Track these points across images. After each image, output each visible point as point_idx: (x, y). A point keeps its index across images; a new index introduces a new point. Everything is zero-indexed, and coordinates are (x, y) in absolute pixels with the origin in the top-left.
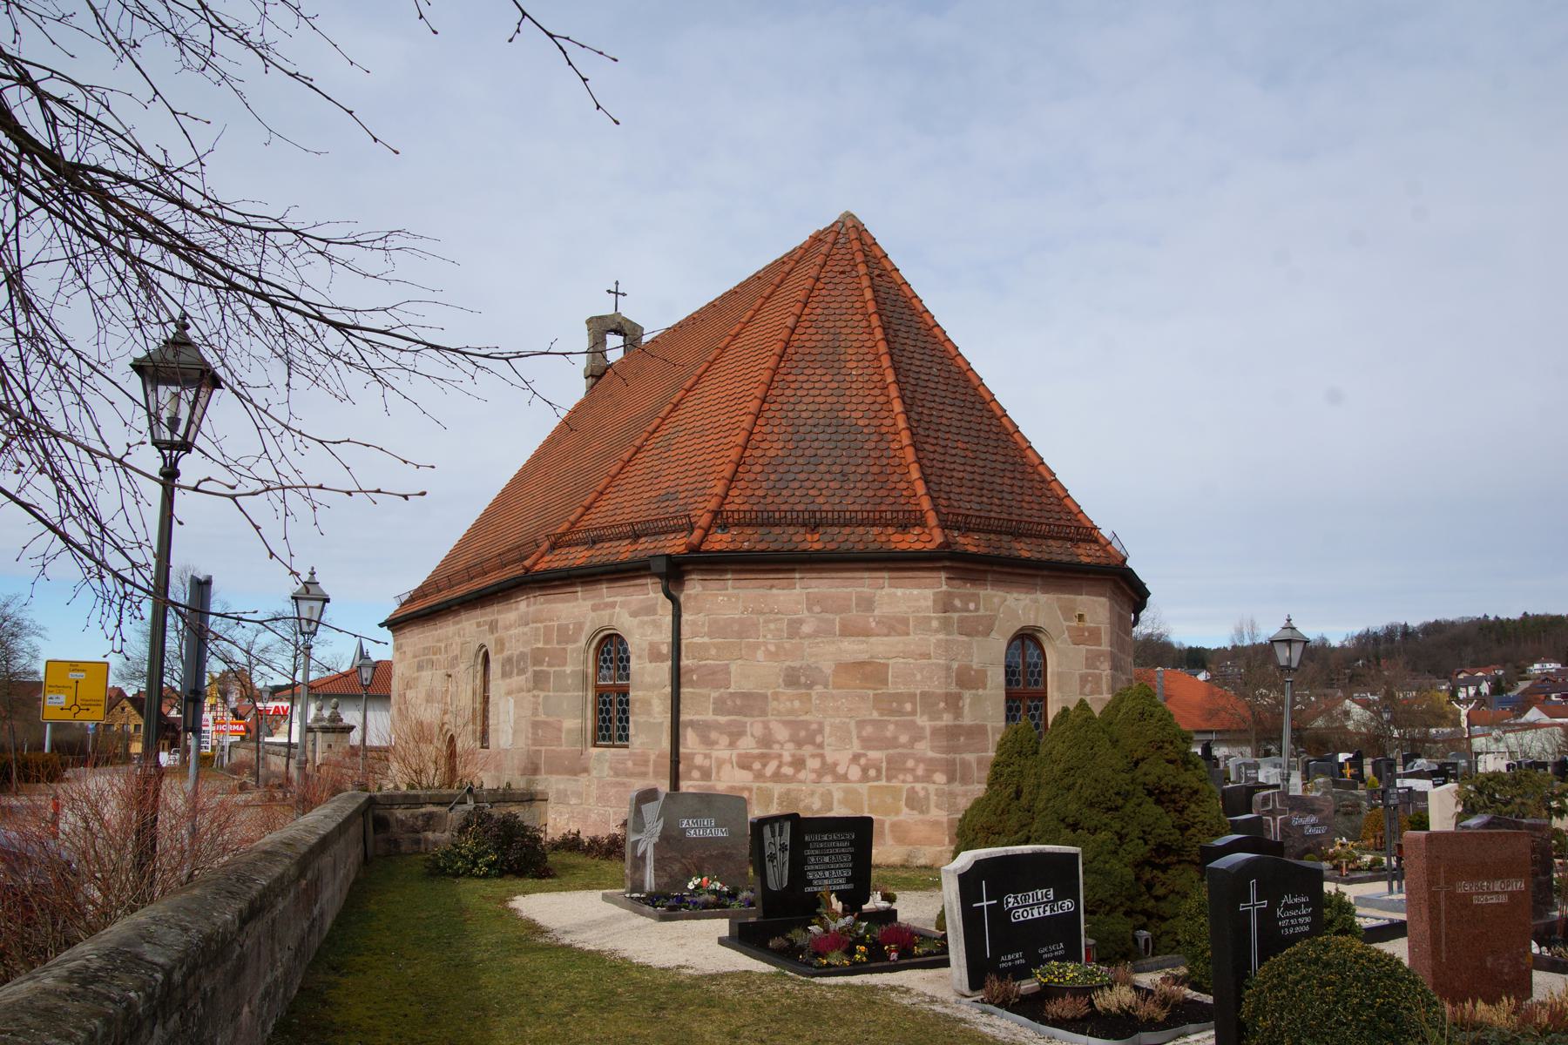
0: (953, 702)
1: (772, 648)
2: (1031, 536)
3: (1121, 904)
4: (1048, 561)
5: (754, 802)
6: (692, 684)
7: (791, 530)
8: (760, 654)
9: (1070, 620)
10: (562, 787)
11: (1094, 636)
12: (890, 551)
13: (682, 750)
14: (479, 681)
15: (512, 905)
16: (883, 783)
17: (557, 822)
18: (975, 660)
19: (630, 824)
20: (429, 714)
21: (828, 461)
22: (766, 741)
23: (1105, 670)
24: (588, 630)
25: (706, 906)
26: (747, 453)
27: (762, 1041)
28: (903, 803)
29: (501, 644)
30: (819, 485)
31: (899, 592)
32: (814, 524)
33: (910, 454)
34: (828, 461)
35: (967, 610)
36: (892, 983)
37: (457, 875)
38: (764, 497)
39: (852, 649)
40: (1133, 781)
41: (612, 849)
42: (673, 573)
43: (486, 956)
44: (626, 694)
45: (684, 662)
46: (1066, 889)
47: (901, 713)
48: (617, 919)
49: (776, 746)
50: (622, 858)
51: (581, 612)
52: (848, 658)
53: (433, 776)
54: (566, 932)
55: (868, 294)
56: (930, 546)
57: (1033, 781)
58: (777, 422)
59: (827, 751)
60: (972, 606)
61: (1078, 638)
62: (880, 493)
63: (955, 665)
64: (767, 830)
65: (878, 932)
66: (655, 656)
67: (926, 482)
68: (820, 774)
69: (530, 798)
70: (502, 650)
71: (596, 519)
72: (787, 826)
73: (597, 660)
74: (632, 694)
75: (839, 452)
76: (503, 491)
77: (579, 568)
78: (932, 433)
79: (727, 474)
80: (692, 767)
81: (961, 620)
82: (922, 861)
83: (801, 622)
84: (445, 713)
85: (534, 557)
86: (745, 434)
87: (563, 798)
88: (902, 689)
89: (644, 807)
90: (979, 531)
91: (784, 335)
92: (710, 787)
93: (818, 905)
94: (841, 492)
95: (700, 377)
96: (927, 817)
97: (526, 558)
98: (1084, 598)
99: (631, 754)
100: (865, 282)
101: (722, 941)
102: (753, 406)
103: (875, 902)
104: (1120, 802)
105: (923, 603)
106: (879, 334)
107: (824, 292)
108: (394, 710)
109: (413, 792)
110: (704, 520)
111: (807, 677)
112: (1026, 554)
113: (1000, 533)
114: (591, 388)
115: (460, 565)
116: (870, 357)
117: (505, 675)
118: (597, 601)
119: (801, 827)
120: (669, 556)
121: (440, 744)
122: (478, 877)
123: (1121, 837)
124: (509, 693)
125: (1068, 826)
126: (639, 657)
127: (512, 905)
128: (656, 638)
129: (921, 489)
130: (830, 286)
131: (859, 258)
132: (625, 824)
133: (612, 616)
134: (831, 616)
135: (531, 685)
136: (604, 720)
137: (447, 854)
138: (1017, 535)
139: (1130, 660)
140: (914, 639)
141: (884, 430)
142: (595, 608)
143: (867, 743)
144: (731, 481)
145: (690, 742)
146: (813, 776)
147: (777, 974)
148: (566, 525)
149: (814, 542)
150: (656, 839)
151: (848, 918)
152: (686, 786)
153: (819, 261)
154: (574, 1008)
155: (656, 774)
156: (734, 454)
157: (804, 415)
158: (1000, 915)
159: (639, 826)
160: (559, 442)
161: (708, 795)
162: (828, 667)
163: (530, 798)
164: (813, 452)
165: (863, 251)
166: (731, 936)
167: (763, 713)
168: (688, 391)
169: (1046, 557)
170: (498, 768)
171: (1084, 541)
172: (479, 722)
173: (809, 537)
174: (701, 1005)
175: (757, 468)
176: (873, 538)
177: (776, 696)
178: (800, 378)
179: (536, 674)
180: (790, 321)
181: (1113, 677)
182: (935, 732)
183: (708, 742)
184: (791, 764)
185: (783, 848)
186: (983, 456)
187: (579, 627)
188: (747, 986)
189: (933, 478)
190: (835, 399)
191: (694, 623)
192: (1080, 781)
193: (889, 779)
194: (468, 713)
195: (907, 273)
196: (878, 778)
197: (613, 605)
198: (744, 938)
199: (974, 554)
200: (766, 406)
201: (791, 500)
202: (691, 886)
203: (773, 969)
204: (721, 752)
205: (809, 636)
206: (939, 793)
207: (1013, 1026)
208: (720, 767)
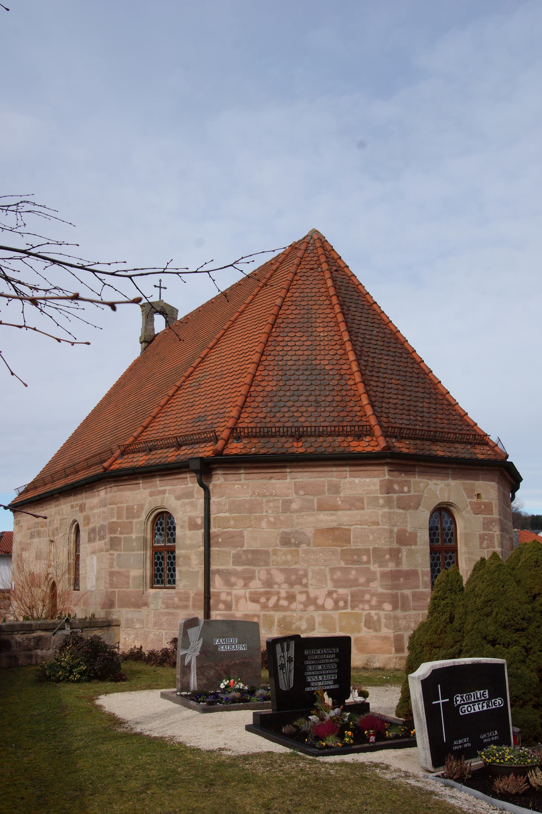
0: (395, 554)
1: (272, 520)
2: (443, 441)
3: (531, 700)
4: (456, 458)
5: (261, 625)
6: (218, 544)
7: (283, 440)
8: (264, 524)
9: (471, 497)
10: (129, 616)
11: (488, 508)
12: (350, 453)
13: (212, 590)
14: (72, 545)
15: (98, 702)
16: (349, 610)
17: (126, 641)
18: (409, 526)
19: (179, 643)
20: (38, 568)
21: (307, 393)
22: (269, 583)
23: (496, 531)
25: (234, 700)
26: (252, 389)
27: (289, 812)
28: (363, 624)
29: (87, 519)
30: (301, 409)
31: (357, 480)
32: (298, 435)
33: (361, 388)
34: (307, 393)
35: (403, 492)
36: (375, 761)
37: (58, 681)
38: (265, 418)
40: (533, 609)
41: (165, 659)
42: (205, 470)
43: (81, 744)
44: (173, 552)
45: (213, 530)
46: (497, 691)
47: (360, 562)
48: (171, 712)
49: (276, 586)
50: (174, 665)
51: (143, 497)
52: (325, 526)
53: (41, 611)
54: (137, 723)
55: (330, 283)
56: (377, 449)
57: (461, 610)
58: (271, 368)
59: (311, 589)
60: (406, 489)
61: (478, 510)
62: (342, 414)
63: (396, 529)
64: (278, 647)
65: (358, 720)
66: (193, 526)
67: (373, 406)
68: (306, 605)
69: (108, 624)
70: (88, 524)
71: (152, 434)
72: (292, 644)
73: (153, 529)
74: (177, 552)
75: (314, 388)
76: (87, 418)
77: (140, 467)
78: (374, 373)
79: (239, 403)
80: (219, 601)
81: (399, 499)
82: (377, 665)
83: (291, 501)
84: (49, 566)
85: (110, 461)
86: (250, 376)
87: (130, 624)
88: (360, 546)
89: (189, 631)
90: (409, 438)
91: (275, 310)
92: (232, 615)
93: (315, 700)
94: (316, 414)
95: (218, 340)
96: (379, 634)
97: (104, 461)
98: (481, 483)
99: (177, 593)
100: (327, 275)
101: (248, 728)
102: (256, 358)
103: (354, 698)
104: (525, 625)
105: (372, 487)
106: (337, 309)
107: (300, 282)
108: (14, 566)
109: (28, 622)
110: (225, 434)
112: (441, 454)
113: (423, 439)
114: (144, 350)
115: (59, 467)
116: (332, 324)
117: (90, 540)
118: (153, 489)
119: (303, 645)
120: (201, 458)
121: (46, 588)
122: (73, 682)
123: (527, 650)
124: (93, 553)
125: (489, 642)
126: (182, 527)
127: (98, 702)
128: (194, 514)
129: (369, 411)
130: (304, 278)
131: (323, 259)
132: (175, 641)
133: (163, 500)
134: (311, 497)
135: (108, 547)
136: (158, 570)
137: (51, 667)
138: (434, 441)
139: (511, 524)
140: (368, 512)
141: (343, 372)
142: (151, 494)
143: (337, 583)
144: (242, 408)
146: (302, 606)
147: (292, 754)
148: (131, 439)
149: (299, 448)
150: (197, 653)
151: (337, 710)
152: (215, 615)
153: (296, 261)
154: (147, 786)
155: (194, 606)
156: (243, 390)
157: (289, 363)
158: (451, 709)
159: (186, 645)
160: (124, 386)
161: (233, 622)
162: (309, 532)
163: (108, 624)
164: (296, 388)
165: (325, 254)
166: (255, 724)
167: (267, 564)
168: (211, 349)
169: (455, 455)
170: (86, 603)
171: (479, 444)
172: (72, 573)
173: (295, 444)
174: (239, 781)
175: (259, 399)
176: (338, 444)
177: (275, 552)
178: (287, 339)
179: (112, 539)
180: (278, 302)
181: (502, 536)
182: (384, 575)
183: (229, 584)
184: (286, 598)
185: (290, 660)
186: (409, 389)
187: (141, 507)
188: (271, 764)
189: (377, 404)
190: (310, 352)
191: (219, 503)
192: (496, 610)
193: (353, 608)
194: (65, 567)
195: (354, 269)
196: (345, 607)
197: (164, 492)
198: (262, 726)
199: (406, 454)
200: (264, 358)
201: (283, 420)
202: (222, 686)
203: (288, 750)
204: (238, 591)
205: (296, 511)
206: (387, 617)
207: (471, 798)
208: (238, 602)
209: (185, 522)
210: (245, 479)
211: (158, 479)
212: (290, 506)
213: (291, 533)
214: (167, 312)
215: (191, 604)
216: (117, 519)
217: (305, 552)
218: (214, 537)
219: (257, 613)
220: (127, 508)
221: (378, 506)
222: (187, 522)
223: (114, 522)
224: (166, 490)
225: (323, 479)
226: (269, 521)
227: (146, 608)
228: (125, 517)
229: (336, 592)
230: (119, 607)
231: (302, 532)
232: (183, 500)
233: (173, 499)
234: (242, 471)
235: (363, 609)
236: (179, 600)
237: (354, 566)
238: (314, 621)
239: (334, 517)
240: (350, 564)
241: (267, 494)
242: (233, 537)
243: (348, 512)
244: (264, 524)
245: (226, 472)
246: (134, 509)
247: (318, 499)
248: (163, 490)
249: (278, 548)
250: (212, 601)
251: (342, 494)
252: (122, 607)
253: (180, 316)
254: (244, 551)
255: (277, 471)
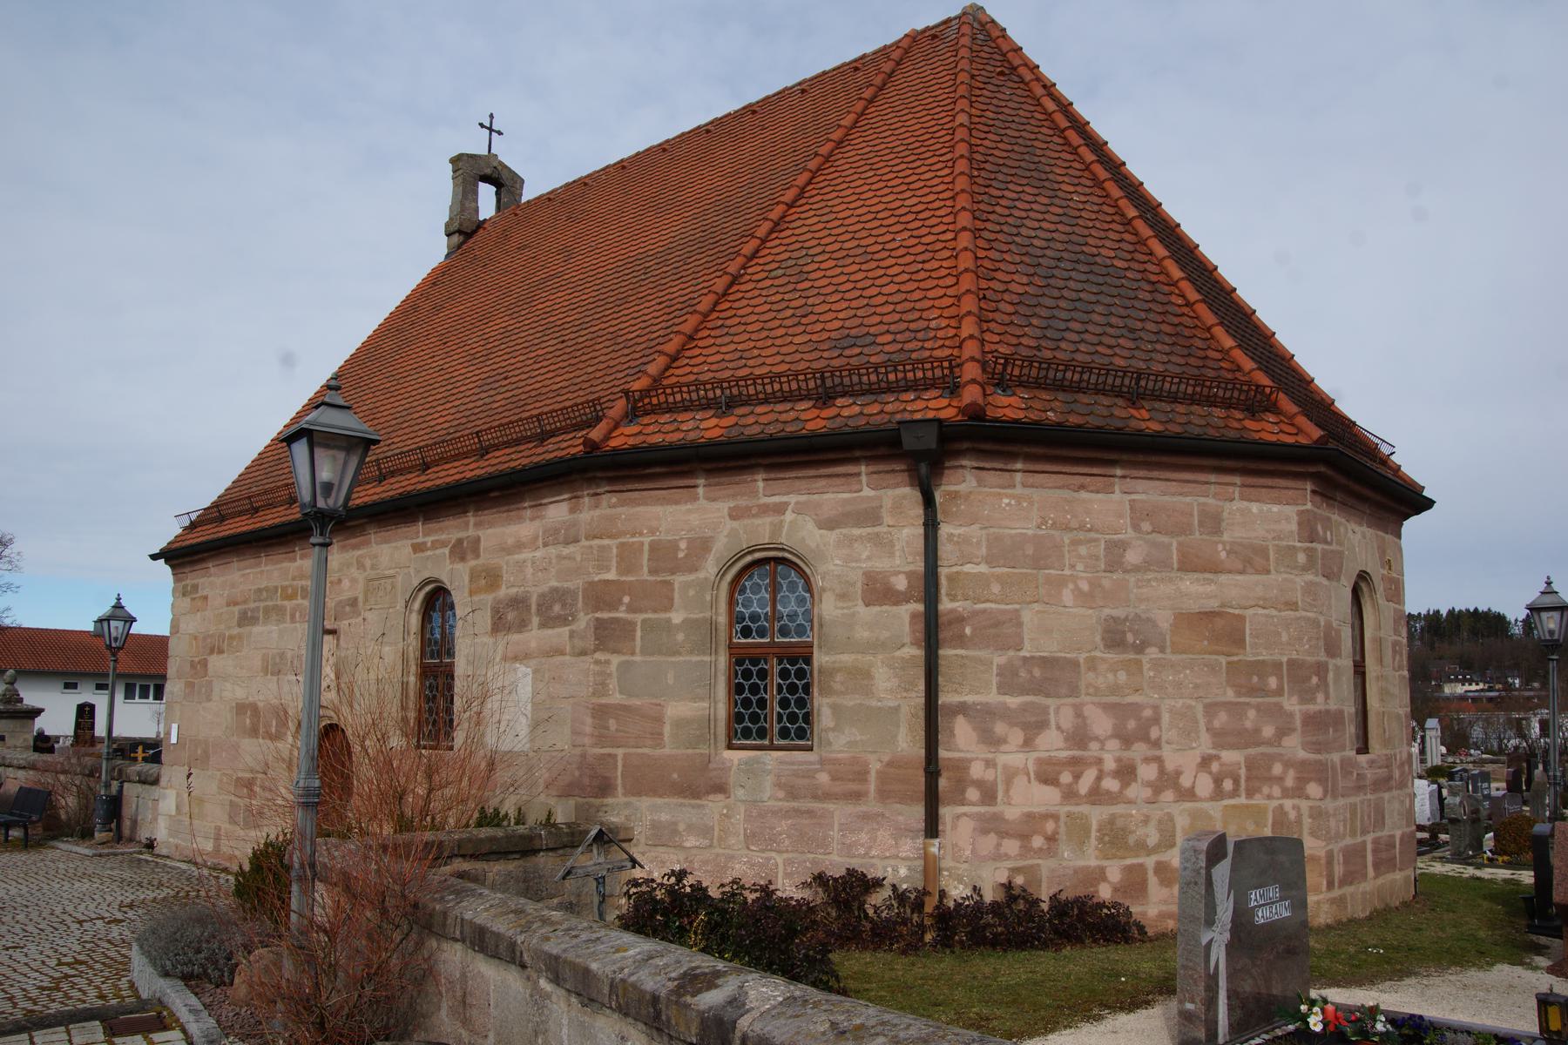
1: (1085, 587)
6: (961, 640)
8: (1067, 596)
10: (664, 817)
13: (943, 753)
16: (1242, 800)
22: (1079, 737)
24: (722, 547)
31: (1255, 507)
39: (1197, 591)
45: (945, 605)
47: (1261, 691)
49: (1094, 746)
51: (708, 521)
52: (1194, 606)
59: (1167, 753)
66: (878, 592)
68: (1157, 788)
74: (820, 659)
83: (1123, 546)
88: (1265, 656)
99: (822, 762)
111: (1136, 633)
118: (742, 502)
128: (881, 564)
133: (777, 529)
135: (591, 642)
142: (735, 515)
143: (1222, 738)
145: (961, 740)
146: (1147, 793)
162: (1164, 619)
167: (1074, 691)
177: (1092, 665)
179: (600, 625)
183: (991, 740)
193: (1250, 794)
196: (1235, 793)
197: (780, 509)
204: (1012, 757)
205: (1136, 569)
209: (853, 584)
210: (1024, 486)
211: (760, 476)
212: (1122, 556)
213: (1126, 619)
214: (503, 180)
215: (872, 787)
216: (621, 572)
217: (1157, 665)
218: (950, 623)
219: (1053, 809)
220: (654, 547)
221: (1295, 568)
222: (859, 585)
223: (607, 581)
224: (787, 504)
225: (1188, 499)
226: (1077, 588)
227: (720, 797)
228: (645, 569)
229: (1218, 758)
230: (625, 795)
231: (1149, 619)
232: (844, 531)
233: (811, 525)
234: (1019, 466)
235: (1269, 797)
236: (834, 779)
237: (1253, 701)
238: (1174, 826)
239: (1213, 587)
240: (1244, 695)
241: (1074, 524)
242: (997, 624)
243: (1240, 577)
244: (1067, 596)
245: (982, 465)
246: (677, 549)
247: (1180, 544)
248: (775, 504)
249: (1098, 654)
250: (943, 783)
251: (1226, 537)
252: (639, 794)
253: (528, 195)
254: (1025, 658)
255: (1095, 471)
